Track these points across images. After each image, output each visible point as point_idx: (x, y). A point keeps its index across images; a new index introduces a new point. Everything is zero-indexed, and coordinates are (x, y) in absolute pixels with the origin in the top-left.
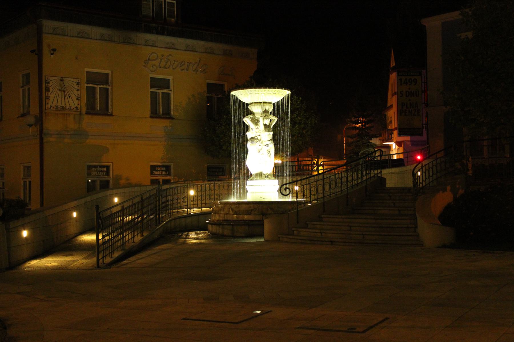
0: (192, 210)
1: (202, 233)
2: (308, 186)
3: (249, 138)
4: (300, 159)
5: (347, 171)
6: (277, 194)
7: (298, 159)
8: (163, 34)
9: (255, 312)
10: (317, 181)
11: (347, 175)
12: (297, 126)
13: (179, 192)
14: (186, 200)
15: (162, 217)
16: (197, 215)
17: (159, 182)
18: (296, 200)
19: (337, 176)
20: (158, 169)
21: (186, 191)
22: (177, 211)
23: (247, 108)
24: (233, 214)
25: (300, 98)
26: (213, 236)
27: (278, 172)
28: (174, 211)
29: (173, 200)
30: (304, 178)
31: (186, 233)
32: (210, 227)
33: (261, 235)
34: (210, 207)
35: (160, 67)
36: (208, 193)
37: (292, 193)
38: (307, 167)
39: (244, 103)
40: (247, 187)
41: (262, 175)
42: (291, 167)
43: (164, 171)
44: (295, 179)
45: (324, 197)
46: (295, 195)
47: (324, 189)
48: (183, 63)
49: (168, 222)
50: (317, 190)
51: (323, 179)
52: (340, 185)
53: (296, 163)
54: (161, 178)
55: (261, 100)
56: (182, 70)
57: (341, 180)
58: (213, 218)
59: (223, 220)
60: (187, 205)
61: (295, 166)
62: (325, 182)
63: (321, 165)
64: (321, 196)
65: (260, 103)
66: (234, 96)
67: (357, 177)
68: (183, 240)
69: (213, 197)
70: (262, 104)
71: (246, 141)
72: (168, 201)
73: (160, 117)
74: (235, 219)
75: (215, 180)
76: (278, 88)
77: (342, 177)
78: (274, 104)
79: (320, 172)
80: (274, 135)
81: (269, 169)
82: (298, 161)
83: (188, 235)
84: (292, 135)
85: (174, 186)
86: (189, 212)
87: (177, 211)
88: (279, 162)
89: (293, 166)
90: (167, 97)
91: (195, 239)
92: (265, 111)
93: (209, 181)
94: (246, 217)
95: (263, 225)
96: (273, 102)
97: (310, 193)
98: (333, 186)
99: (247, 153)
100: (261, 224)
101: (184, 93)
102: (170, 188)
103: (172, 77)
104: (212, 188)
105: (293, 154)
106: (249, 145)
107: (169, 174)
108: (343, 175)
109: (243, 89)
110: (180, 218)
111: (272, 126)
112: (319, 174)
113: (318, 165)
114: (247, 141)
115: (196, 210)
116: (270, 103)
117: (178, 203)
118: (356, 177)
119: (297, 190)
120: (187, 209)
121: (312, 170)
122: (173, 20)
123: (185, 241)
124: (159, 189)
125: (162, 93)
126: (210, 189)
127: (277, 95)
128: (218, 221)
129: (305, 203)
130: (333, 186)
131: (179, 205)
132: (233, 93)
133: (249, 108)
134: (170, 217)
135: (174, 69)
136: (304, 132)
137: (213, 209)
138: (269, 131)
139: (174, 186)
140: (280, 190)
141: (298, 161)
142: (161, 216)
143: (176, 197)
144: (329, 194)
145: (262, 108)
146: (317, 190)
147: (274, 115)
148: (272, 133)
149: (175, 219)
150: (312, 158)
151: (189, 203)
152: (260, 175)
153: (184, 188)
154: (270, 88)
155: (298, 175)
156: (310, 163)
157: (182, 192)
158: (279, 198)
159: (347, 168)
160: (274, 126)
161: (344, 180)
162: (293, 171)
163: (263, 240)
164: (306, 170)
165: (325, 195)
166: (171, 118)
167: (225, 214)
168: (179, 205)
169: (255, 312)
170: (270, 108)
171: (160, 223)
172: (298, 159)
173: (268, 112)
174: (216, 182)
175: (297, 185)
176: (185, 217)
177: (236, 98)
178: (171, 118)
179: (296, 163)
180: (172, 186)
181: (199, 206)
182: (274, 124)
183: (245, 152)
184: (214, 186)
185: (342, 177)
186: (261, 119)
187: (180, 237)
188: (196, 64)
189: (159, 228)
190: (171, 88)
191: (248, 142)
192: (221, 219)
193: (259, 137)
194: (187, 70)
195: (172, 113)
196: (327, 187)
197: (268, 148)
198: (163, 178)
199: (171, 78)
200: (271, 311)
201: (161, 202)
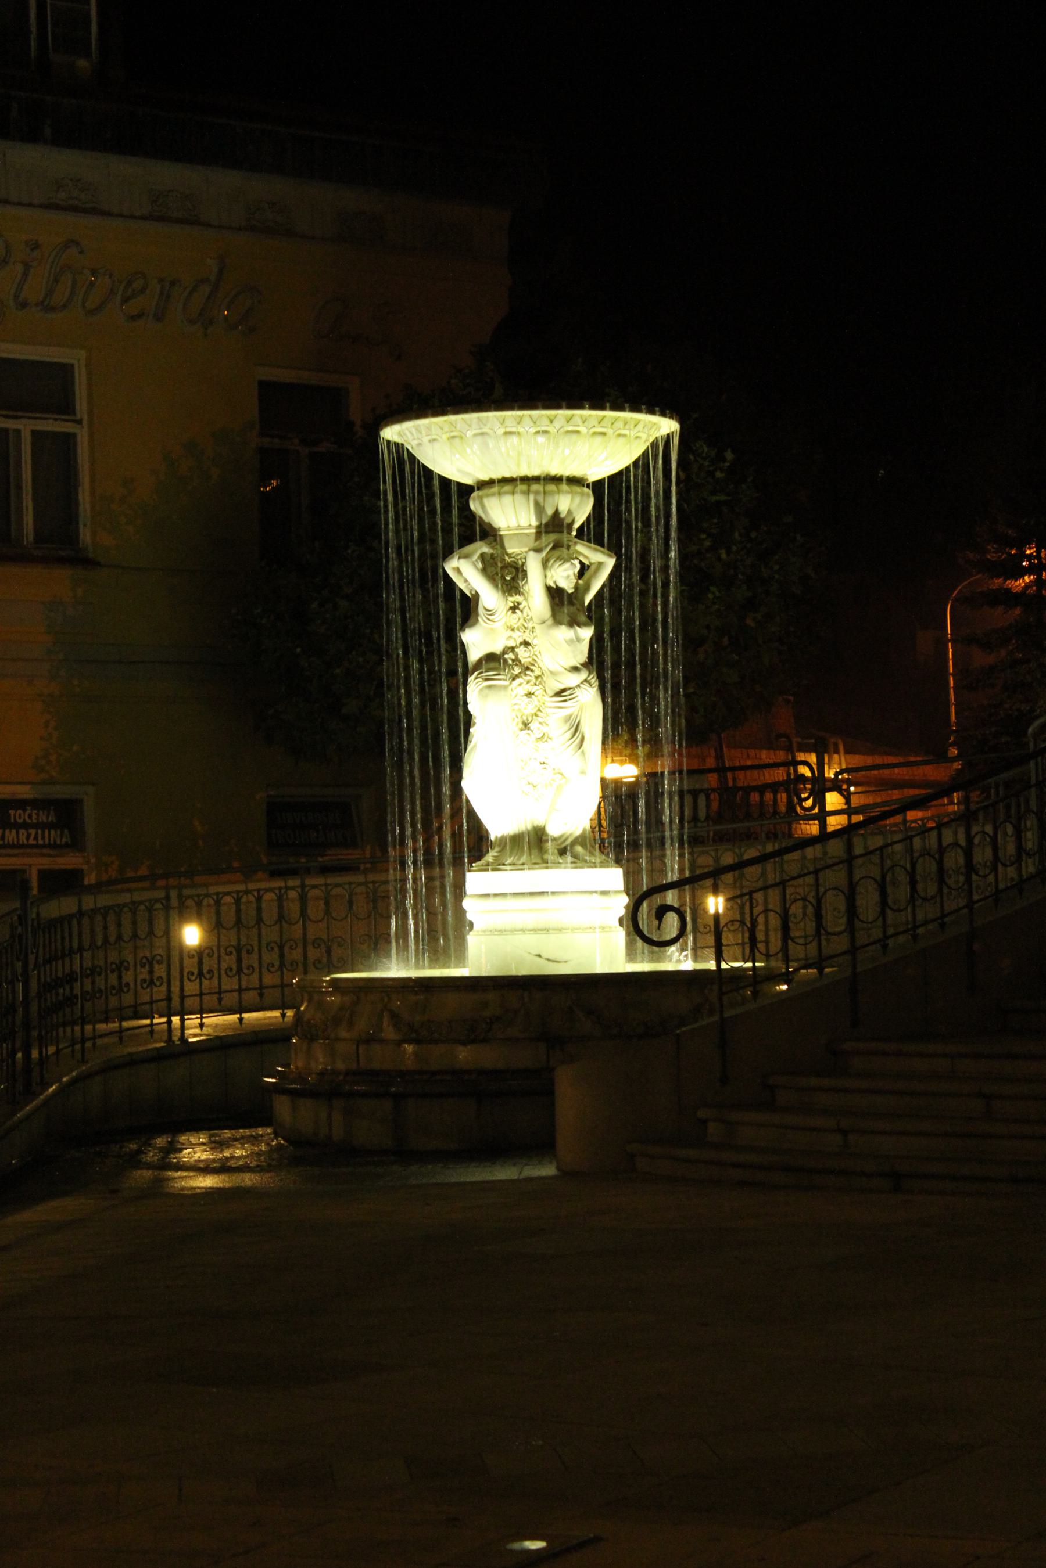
0: (192, 1021)
1: (243, 1140)
2: (774, 895)
3: (474, 655)
4: (734, 757)
5: (967, 818)
6: (620, 936)
7: (719, 757)
8: (32, 136)
9: (516, 1546)
10: (816, 872)
11: (970, 839)
12: (714, 592)
13: (127, 932)
14: (160, 971)
15: (43, 1061)
16: (218, 1046)
17: (25, 885)
18: (712, 965)
19: (917, 842)
20: (17, 815)
21: (159, 930)
22: (114, 1026)
23: (465, 508)
24: (399, 1043)
25: (729, 455)
26: (300, 1152)
27: (622, 827)
28: (102, 1027)
29: (93, 972)
30: (751, 853)
31: (161, 1141)
32: (282, 1107)
33: (542, 1146)
34: (283, 1006)
35: (24, 305)
36: (271, 934)
37: (695, 930)
38: (769, 796)
39: (445, 482)
40: (466, 903)
41: (541, 843)
42: (688, 799)
43: (51, 826)
44: (706, 861)
45: (853, 951)
46: (711, 940)
47: (852, 911)
48: (137, 284)
49: (74, 1082)
50: (818, 916)
51: (849, 860)
52: (932, 889)
53: (713, 779)
54: (34, 864)
55: (532, 461)
56: (133, 318)
57: (940, 863)
58: (298, 1063)
59: (347, 1073)
60: (169, 999)
61: (707, 793)
62: (857, 876)
63: (836, 786)
64: (841, 944)
65: (525, 480)
66: (399, 448)
67: (1020, 848)
68: (147, 1174)
69: (297, 954)
70: (535, 487)
71: (456, 669)
72: (71, 978)
73: (23, 558)
74: (410, 1064)
75: (308, 871)
76: (617, 407)
77: (942, 850)
78: (597, 487)
79: (834, 823)
80: (596, 645)
81: (575, 812)
82: (721, 770)
83: (174, 1148)
84: (691, 643)
85: (104, 900)
86: (176, 1035)
87: (114, 1026)
88: (628, 771)
89: (695, 793)
90: (57, 455)
91: (205, 1169)
92: (553, 526)
93: (274, 874)
94: (464, 1055)
95: (549, 1092)
96: (593, 477)
97: (785, 928)
98: (900, 893)
99: (467, 733)
100: (539, 1087)
101: (143, 430)
102: (81, 913)
103: (83, 354)
104: (293, 908)
105: (697, 733)
106: (479, 697)
107: (76, 844)
108: (948, 837)
109: (443, 413)
110: (133, 1062)
111: (589, 598)
112: (825, 836)
113: (820, 786)
114: (466, 675)
115: (213, 1020)
116: (575, 481)
117: (121, 988)
118: (1011, 848)
119: (717, 917)
120: (169, 1016)
121: (792, 815)
122: (82, 63)
123: (160, 1181)
124: (22, 919)
125: (34, 433)
126: (281, 918)
127: (608, 442)
128: (322, 1074)
129: (757, 980)
130: (900, 893)
131: (128, 999)
132: (391, 433)
133: (474, 505)
134: (84, 1061)
135: (92, 312)
136: (749, 622)
137: (298, 1016)
138: (573, 623)
139: (104, 900)
140: (632, 921)
141: (721, 770)
142: (35, 1054)
143: (113, 956)
144: (877, 933)
145: (539, 509)
146: (818, 916)
147: (598, 541)
148: (587, 633)
149: (110, 1068)
150: (789, 749)
151: (175, 989)
152: (534, 844)
153: (150, 910)
154: (575, 404)
155: (721, 838)
156: (780, 774)
157: (142, 930)
158: (631, 954)
159: (966, 801)
160: (599, 594)
161: (954, 860)
162: (695, 819)
163: (548, 1170)
164: (762, 815)
165: (862, 938)
166: (82, 560)
167: (359, 1042)
168: (128, 999)
169: (516, 1546)
170: (579, 508)
171: (30, 1093)
172: (719, 757)
173: (570, 526)
174: (309, 882)
175: (716, 891)
176: (158, 1057)
177: (404, 460)
178: (82, 560)
179: (712, 780)
180: (89, 902)
181: (230, 999)
182: (597, 584)
183: (460, 725)
184: (303, 898)
185: (942, 850)
186: (533, 565)
187: (134, 1161)
188: (206, 289)
189: (28, 1117)
190: (81, 406)
191: (471, 679)
192: (340, 1065)
193: (523, 653)
194: (159, 318)
195: (85, 535)
196: (868, 900)
197: (571, 708)
198: (46, 863)
199: (76, 357)
200: (597, 1539)
201: (34, 985)
